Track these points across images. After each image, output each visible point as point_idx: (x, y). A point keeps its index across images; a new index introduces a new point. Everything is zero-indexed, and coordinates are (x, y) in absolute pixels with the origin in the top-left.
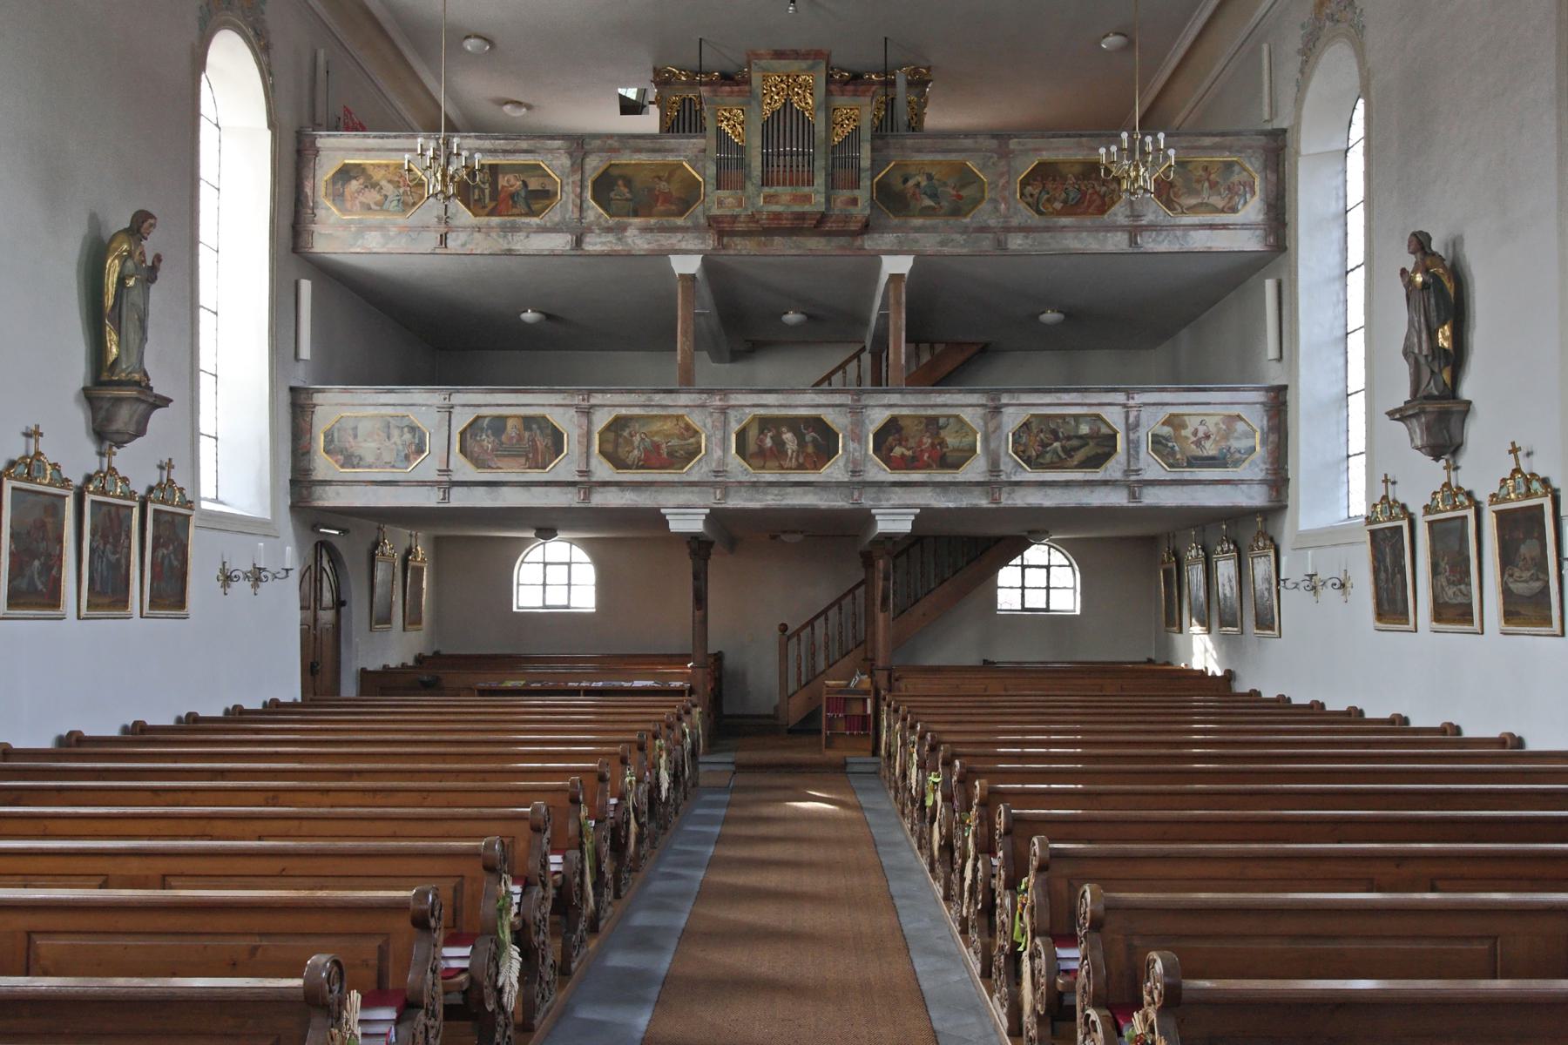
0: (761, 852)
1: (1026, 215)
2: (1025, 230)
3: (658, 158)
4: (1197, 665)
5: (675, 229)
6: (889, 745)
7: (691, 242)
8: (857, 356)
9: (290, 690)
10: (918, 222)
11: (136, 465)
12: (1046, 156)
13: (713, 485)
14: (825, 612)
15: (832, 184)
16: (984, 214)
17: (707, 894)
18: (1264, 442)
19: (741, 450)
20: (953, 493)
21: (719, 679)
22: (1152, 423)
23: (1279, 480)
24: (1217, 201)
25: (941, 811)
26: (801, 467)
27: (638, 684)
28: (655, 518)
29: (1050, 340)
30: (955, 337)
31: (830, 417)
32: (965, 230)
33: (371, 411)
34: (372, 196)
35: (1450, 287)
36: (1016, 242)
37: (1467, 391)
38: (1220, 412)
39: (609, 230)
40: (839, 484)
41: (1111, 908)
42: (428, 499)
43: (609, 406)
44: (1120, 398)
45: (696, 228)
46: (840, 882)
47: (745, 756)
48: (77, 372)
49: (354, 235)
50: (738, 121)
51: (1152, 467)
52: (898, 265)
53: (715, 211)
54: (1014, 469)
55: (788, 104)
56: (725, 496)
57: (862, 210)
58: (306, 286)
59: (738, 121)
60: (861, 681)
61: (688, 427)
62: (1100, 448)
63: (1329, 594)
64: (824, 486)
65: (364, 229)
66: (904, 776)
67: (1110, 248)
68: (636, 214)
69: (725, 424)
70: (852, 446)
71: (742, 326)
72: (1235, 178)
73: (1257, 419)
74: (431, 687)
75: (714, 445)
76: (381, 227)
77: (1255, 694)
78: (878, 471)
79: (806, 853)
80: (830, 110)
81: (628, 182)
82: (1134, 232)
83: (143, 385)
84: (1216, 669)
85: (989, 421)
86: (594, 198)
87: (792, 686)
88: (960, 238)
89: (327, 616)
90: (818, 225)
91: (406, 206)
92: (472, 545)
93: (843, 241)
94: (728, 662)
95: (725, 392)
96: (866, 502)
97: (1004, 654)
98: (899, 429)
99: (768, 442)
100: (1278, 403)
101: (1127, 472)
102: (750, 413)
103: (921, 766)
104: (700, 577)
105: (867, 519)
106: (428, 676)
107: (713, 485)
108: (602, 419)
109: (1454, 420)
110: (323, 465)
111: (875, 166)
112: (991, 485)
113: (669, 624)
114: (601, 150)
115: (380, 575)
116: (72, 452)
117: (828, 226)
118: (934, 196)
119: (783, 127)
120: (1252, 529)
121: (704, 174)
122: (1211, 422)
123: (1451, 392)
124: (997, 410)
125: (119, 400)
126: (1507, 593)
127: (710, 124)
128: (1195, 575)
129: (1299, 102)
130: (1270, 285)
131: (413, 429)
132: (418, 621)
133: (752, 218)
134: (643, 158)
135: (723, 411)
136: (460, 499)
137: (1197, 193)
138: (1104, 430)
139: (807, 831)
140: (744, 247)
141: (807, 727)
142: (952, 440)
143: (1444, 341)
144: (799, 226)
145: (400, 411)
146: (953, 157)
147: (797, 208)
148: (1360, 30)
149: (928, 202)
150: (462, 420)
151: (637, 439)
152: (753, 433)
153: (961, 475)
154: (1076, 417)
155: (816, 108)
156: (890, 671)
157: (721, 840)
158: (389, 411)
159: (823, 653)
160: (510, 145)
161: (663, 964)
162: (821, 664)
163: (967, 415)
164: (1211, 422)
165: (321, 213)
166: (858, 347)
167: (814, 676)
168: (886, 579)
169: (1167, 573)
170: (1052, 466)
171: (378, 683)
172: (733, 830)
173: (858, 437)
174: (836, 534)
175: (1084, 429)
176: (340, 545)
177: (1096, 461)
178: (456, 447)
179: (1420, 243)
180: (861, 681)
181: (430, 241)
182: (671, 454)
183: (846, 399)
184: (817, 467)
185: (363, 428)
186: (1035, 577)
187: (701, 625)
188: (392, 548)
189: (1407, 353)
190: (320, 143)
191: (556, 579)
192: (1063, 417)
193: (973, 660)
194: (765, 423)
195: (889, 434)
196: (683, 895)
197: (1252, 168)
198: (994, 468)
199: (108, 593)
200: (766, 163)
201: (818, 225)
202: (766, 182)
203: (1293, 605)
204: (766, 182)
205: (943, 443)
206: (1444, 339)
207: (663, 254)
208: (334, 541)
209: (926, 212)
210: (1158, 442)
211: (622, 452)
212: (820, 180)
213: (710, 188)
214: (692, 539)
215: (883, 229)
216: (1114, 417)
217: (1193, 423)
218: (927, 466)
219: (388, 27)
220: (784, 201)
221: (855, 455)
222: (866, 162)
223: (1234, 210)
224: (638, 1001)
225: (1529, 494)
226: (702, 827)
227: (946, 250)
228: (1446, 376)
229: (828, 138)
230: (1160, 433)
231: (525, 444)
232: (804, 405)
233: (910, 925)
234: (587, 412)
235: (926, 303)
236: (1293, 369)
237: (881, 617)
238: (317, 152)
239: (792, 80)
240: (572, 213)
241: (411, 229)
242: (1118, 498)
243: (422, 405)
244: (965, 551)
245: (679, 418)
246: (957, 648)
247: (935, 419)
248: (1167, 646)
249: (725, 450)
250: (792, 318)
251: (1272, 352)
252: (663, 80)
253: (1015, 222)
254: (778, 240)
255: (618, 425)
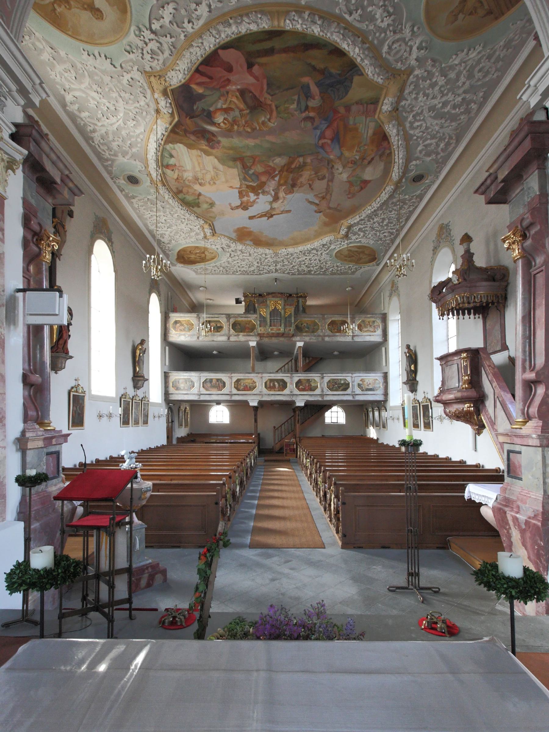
0: (273, 477)
1: (328, 332)
2: (329, 336)
3: (246, 319)
4: (371, 437)
5: (251, 336)
6: (300, 455)
7: (254, 338)
8: (291, 360)
9: (165, 443)
10: (304, 334)
11: (140, 393)
12: (333, 319)
13: (259, 395)
14: (284, 423)
15: (285, 326)
16: (319, 332)
17: (263, 484)
18: (383, 385)
19: (266, 387)
20: (314, 397)
21: (259, 440)
22: (357, 380)
23: (386, 394)
24: (372, 329)
25: (309, 467)
26: (279, 391)
27: (242, 441)
28: (246, 403)
29: (336, 357)
30: (313, 359)
31: (285, 379)
32: (315, 336)
33: (182, 377)
34: (182, 328)
35: (413, 357)
36: (327, 339)
37: (418, 379)
38: (373, 378)
39: (236, 336)
40: (288, 395)
41: (331, 475)
42: (195, 398)
43: (236, 376)
44: (350, 375)
45: (255, 335)
46: (290, 482)
47: (267, 458)
48: (131, 374)
49: (179, 337)
50: (264, 312)
51: (358, 391)
52: (300, 344)
53: (260, 332)
54: (327, 391)
55: (275, 308)
56: (262, 397)
57: (292, 332)
58: (167, 348)
59: (264, 312)
60: (293, 440)
61: (254, 381)
62: (345, 386)
63: (396, 421)
64: (284, 395)
65: (180, 335)
66: (303, 461)
67: (348, 340)
68: (241, 332)
69: (262, 380)
70: (291, 386)
71: (264, 354)
72: (375, 324)
73: (381, 380)
74: (193, 441)
75: (259, 385)
76: (184, 335)
77: (383, 443)
78: (296, 392)
79: (282, 477)
80: (285, 309)
81: (240, 324)
82: (353, 336)
83: (143, 377)
84: (375, 438)
85: (321, 381)
86: (232, 328)
87: (277, 441)
88: (314, 338)
89: (170, 424)
90: (283, 335)
91: (190, 330)
92: (200, 407)
93: (287, 338)
94: (261, 436)
95: (262, 373)
96: (294, 399)
97: (328, 433)
98: (301, 382)
99: (272, 385)
100: (386, 376)
101: (352, 392)
102: (268, 378)
103: (306, 459)
104: (256, 415)
105: (293, 402)
106: (191, 438)
107: (259, 395)
108: (234, 380)
109: (415, 385)
110: (171, 390)
111: (295, 322)
112: (322, 395)
113: (247, 425)
114: (233, 317)
115: (181, 415)
116: (131, 392)
117: (285, 335)
118: (308, 328)
119: (274, 313)
120: (381, 405)
121: (257, 323)
122: (371, 380)
123: (415, 379)
124: (323, 378)
125: (139, 380)
126: (424, 422)
127: (258, 312)
128: (371, 415)
129: (389, 307)
130: (383, 349)
131: (192, 382)
132: (187, 426)
133: (268, 334)
134: (243, 319)
135: (262, 377)
136: (203, 398)
137: (367, 328)
138: (347, 382)
139: (281, 474)
140: (266, 340)
141: (280, 451)
142: (313, 385)
143: (413, 369)
144: (278, 335)
145: (189, 377)
146: (313, 319)
147: (278, 332)
148: (399, 295)
149: (307, 329)
150: (203, 380)
151: (242, 384)
152: (268, 383)
153: (315, 393)
154: (341, 379)
155: (282, 309)
156: (300, 438)
157: (264, 475)
158: (186, 377)
159: (284, 435)
160: (213, 316)
161: (258, 495)
162: (283, 436)
163: (316, 379)
164: (371, 380)
165: (171, 331)
166: (290, 359)
167: (282, 439)
168: (299, 416)
169: (365, 414)
170: (336, 390)
171: (181, 440)
172: (265, 473)
173: (292, 384)
174: (288, 405)
175: (342, 382)
176: (173, 408)
177: (345, 389)
178: (202, 386)
179: (408, 347)
180: (293, 440)
181: (195, 338)
182: (250, 387)
183: (289, 375)
184: (283, 391)
185: (180, 381)
186: (334, 415)
187: (256, 427)
188: (182, 408)
189: (406, 370)
190: (170, 315)
191: (219, 415)
192: (338, 379)
193: (320, 435)
194: (271, 380)
195: (299, 383)
196: (259, 485)
197: (379, 322)
198: (322, 391)
199: (137, 423)
200: (270, 321)
201: (283, 335)
202: (270, 326)
203: (390, 422)
204: (270, 326)
205: (311, 385)
206: (413, 367)
207: (248, 341)
208: (173, 406)
209: (306, 332)
210: (359, 385)
211: (239, 387)
212: (283, 325)
213: (258, 327)
214: (254, 407)
215: (297, 336)
216: (349, 379)
217: (367, 381)
218: (307, 390)
219: (183, 285)
220: (275, 330)
221: (291, 387)
222: (293, 321)
223: (375, 332)
224: (255, 500)
225: (427, 402)
226: (260, 473)
227: (311, 341)
228: (413, 375)
229: (284, 316)
230: (360, 383)
231: (217, 385)
232: (279, 376)
233: (303, 489)
234: (231, 378)
235: (306, 352)
236: (388, 369)
237: (298, 425)
238: (169, 317)
239: (276, 302)
240: (227, 332)
241: (191, 335)
242: (350, 398)
243: (194, 376)
244: (318, 409)
245: (251, 379)
246: (316, 432)
247: (309, 380)
248: (365, 432)
249: (262, 387)
250: (276, 353)
251: (384, 364)
252: (245, 296)
253: (326, 334)
254: (273, 338)
255: (238, 381)
